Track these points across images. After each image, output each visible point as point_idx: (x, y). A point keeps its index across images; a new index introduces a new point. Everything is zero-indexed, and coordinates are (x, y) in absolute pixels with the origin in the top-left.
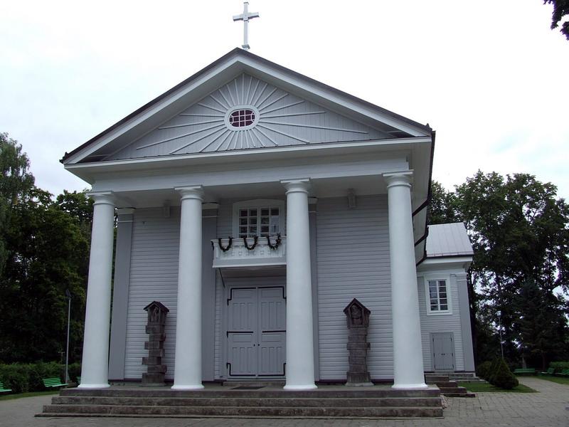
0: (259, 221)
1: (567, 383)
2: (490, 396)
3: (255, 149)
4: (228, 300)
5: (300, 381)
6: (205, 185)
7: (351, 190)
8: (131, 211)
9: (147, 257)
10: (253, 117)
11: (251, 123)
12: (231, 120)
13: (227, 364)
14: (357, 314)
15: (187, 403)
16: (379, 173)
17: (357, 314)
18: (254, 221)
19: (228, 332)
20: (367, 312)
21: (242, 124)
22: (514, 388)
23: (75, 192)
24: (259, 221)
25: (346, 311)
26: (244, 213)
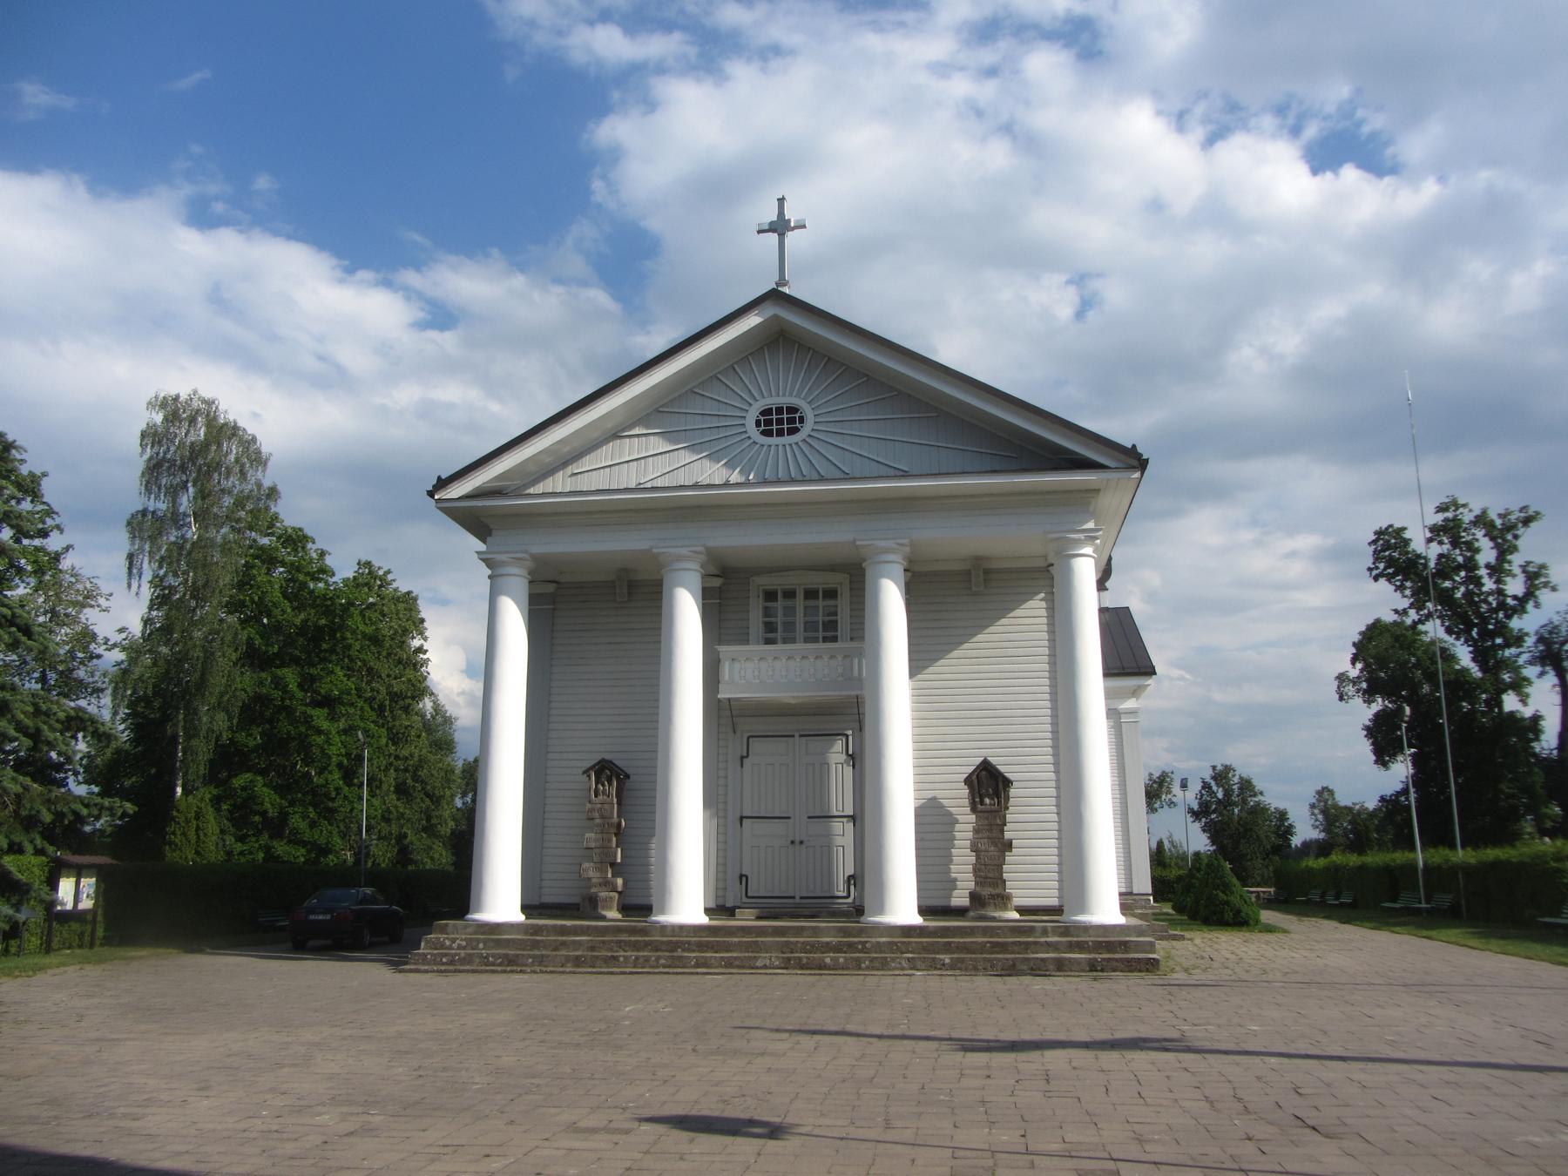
0: (800, 611)
1: (1564, 945)
2: (1267, 943)
3: (627, 490)
4: (742, 758)
5: (902, 905)
6: (712, 543)
7: (625, 570)
8: (551, 588)
9: (1029, 728)
10: (802, 420)
11: (796, 430)
12: (758, 423)
13: (741, 876)
14: (989, 784)
15: (688, 947)
16: (644, 545)
17: (989, 784)
18: (790, 611)
19: (742, 818)
20: (1007, 783)
21: (780, 433)
22: (465, 750)
23: (1404, 529)
24: (800, 611)
25: (968, 781)
26: (770, 596)
